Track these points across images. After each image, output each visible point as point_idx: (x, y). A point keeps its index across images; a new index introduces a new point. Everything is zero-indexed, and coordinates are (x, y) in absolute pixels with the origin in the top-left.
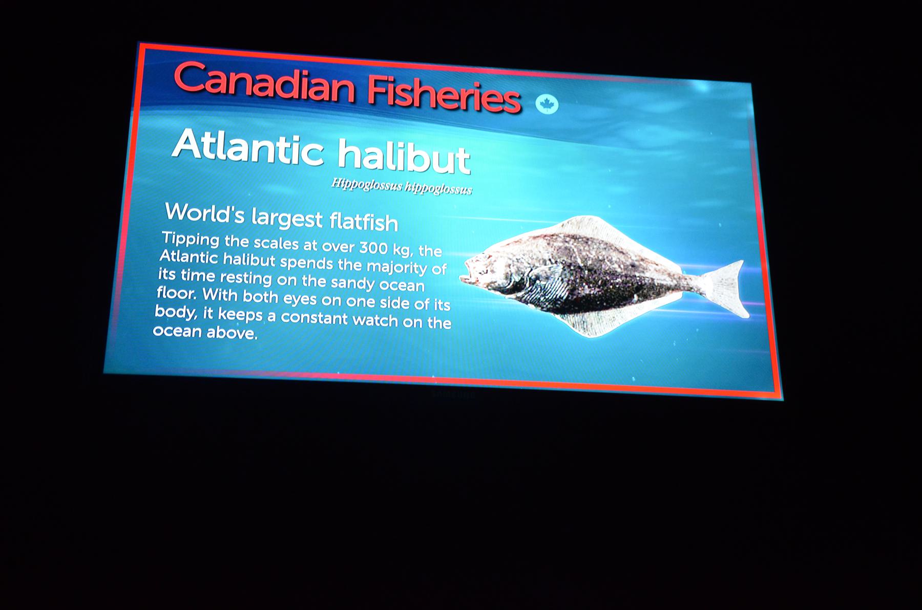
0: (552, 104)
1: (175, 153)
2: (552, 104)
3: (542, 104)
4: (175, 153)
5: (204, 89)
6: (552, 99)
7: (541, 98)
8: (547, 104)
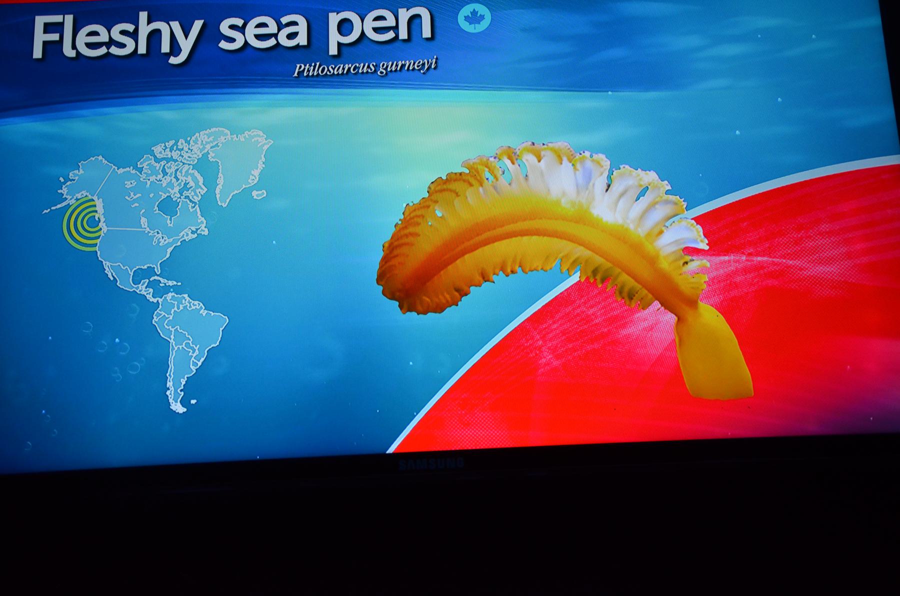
0: (482, 17)
1: (38, 53)
2: (482, 17)
3: (467, 18)
4: (38, 53)
6: (482, 9)
7: (466, 11)
8: (474, 18)
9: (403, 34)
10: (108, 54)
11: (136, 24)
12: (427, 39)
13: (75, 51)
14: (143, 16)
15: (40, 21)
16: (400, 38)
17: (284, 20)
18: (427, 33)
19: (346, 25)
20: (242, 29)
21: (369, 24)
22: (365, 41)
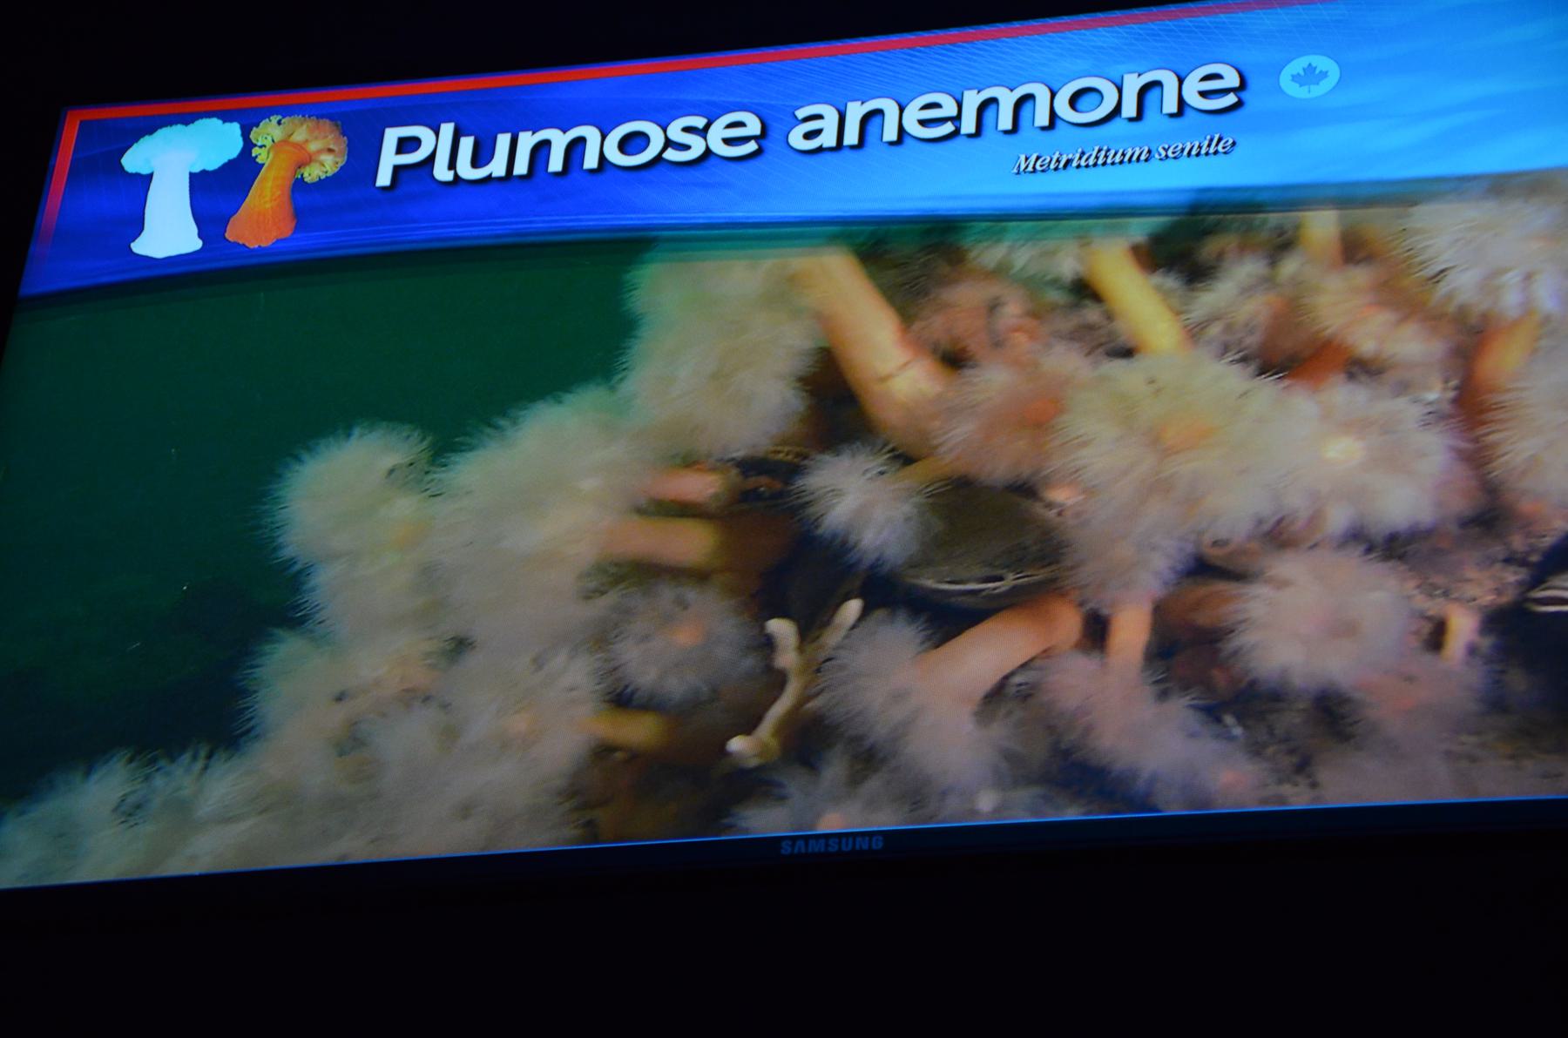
0: (1324, 75)
1: (384, 178)
3: (1295, 78)
5: (708, 152)
6: (1322, 63)
7: (1297, 66)
8: (1310, 76)
9: (968, 125)
13: (452, 173)
15: (392, 135)
16: (963, 131)
18: (1006, 122)
19: (639, 141)
20: (703, 132)
21: (913, 114)
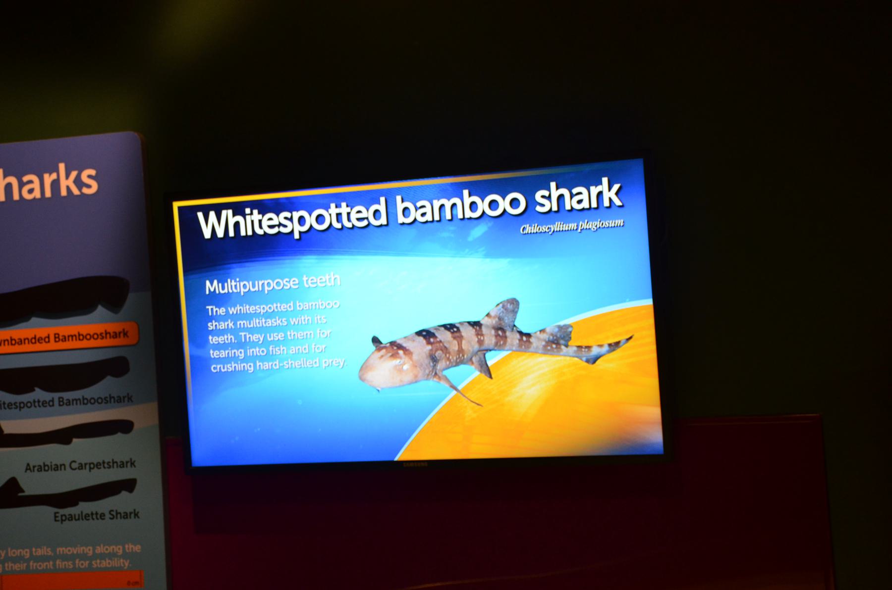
10: (279, 232)
11: (549, 190)
12: (607, 207)
14: (553, 185)
17: (419, 204)
18: (449, 217)
19: (320, 218)
22: (416, 223)
